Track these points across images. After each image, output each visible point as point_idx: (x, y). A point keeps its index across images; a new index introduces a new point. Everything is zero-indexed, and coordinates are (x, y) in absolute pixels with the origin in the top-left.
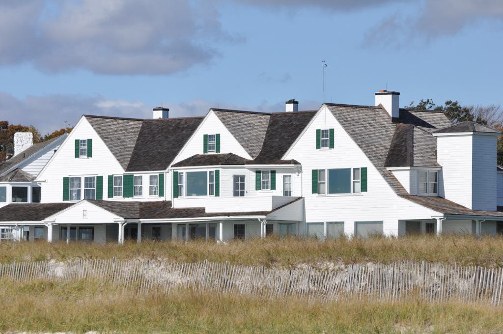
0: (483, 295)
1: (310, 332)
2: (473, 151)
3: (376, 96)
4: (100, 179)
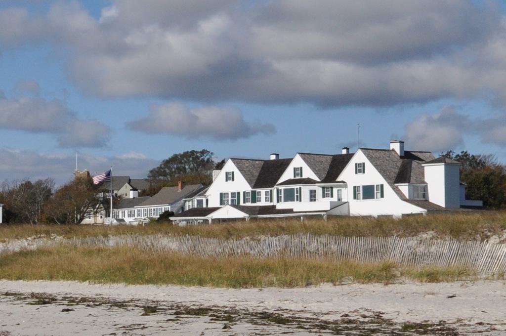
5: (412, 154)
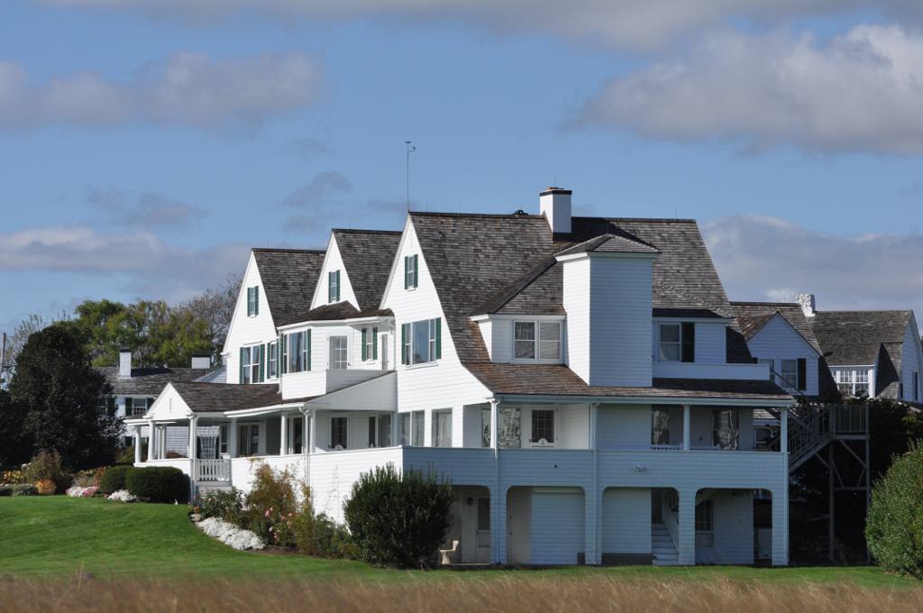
0: (327, 569)
1: (887, 610)
2: (591, 285)
3: (542, 198)
4: (263, 346)
5: (569, 241)
